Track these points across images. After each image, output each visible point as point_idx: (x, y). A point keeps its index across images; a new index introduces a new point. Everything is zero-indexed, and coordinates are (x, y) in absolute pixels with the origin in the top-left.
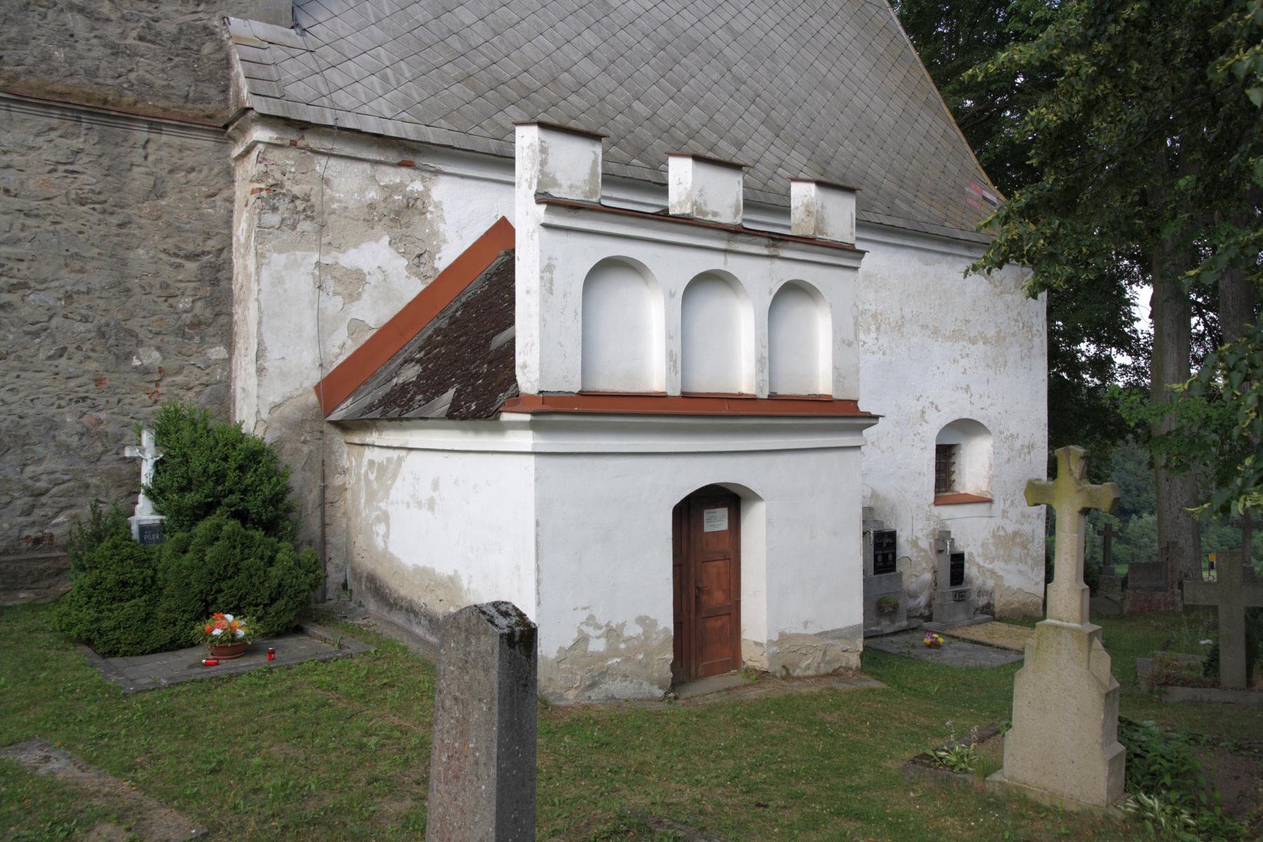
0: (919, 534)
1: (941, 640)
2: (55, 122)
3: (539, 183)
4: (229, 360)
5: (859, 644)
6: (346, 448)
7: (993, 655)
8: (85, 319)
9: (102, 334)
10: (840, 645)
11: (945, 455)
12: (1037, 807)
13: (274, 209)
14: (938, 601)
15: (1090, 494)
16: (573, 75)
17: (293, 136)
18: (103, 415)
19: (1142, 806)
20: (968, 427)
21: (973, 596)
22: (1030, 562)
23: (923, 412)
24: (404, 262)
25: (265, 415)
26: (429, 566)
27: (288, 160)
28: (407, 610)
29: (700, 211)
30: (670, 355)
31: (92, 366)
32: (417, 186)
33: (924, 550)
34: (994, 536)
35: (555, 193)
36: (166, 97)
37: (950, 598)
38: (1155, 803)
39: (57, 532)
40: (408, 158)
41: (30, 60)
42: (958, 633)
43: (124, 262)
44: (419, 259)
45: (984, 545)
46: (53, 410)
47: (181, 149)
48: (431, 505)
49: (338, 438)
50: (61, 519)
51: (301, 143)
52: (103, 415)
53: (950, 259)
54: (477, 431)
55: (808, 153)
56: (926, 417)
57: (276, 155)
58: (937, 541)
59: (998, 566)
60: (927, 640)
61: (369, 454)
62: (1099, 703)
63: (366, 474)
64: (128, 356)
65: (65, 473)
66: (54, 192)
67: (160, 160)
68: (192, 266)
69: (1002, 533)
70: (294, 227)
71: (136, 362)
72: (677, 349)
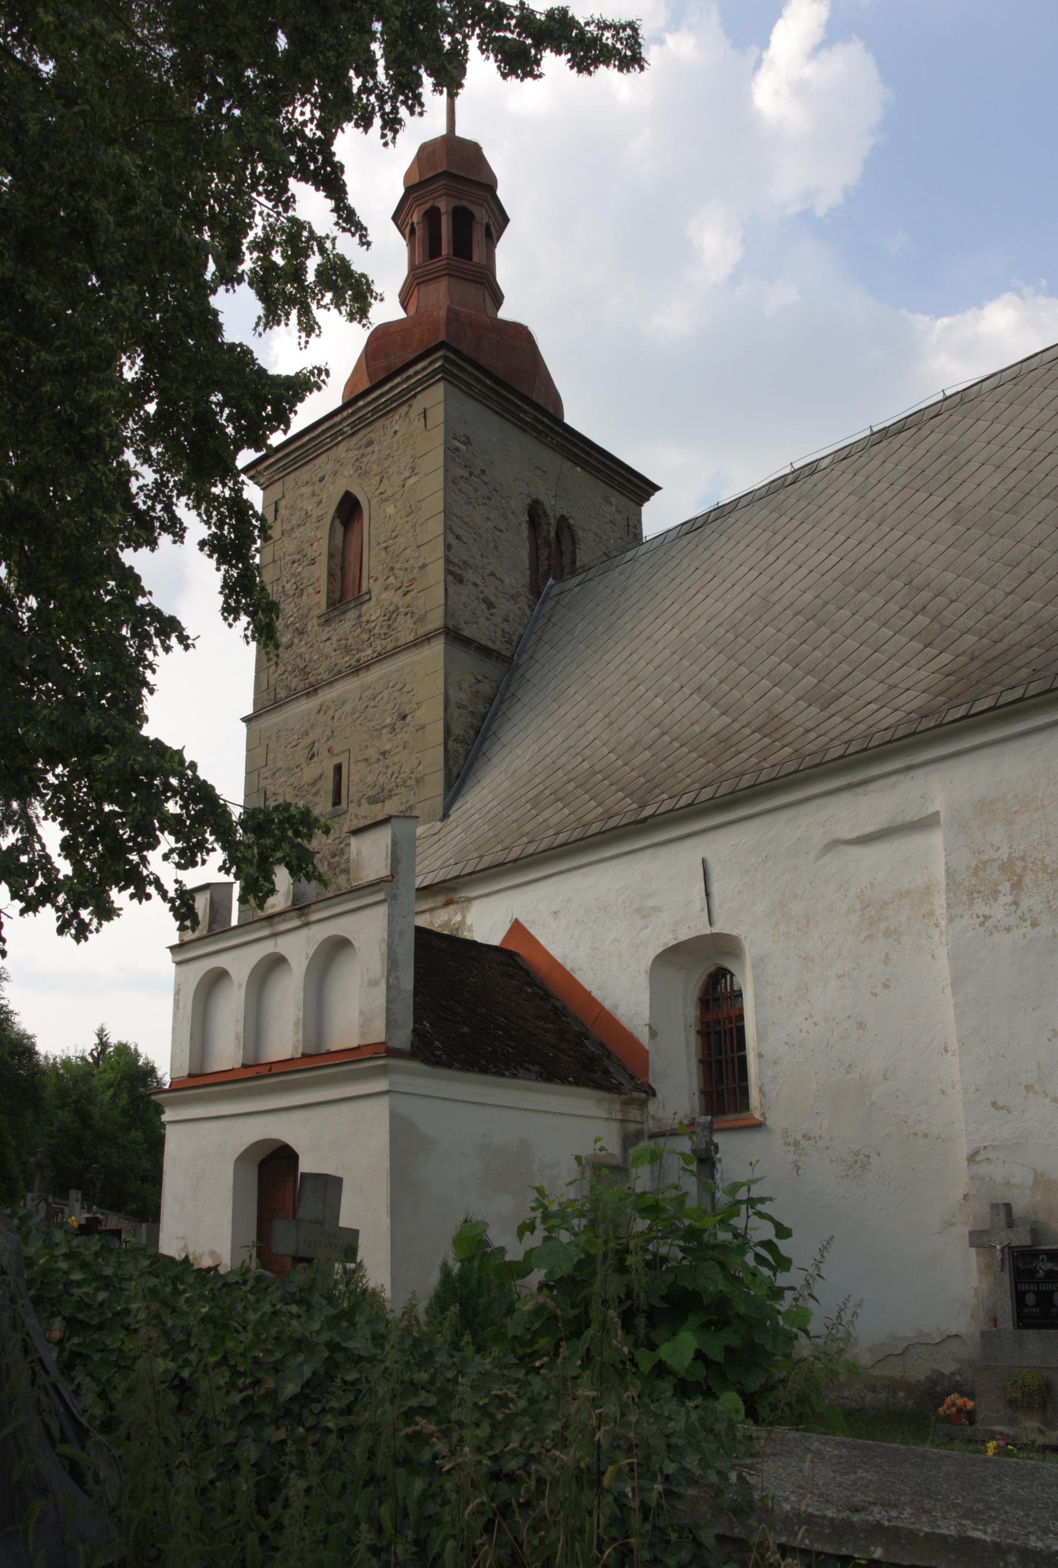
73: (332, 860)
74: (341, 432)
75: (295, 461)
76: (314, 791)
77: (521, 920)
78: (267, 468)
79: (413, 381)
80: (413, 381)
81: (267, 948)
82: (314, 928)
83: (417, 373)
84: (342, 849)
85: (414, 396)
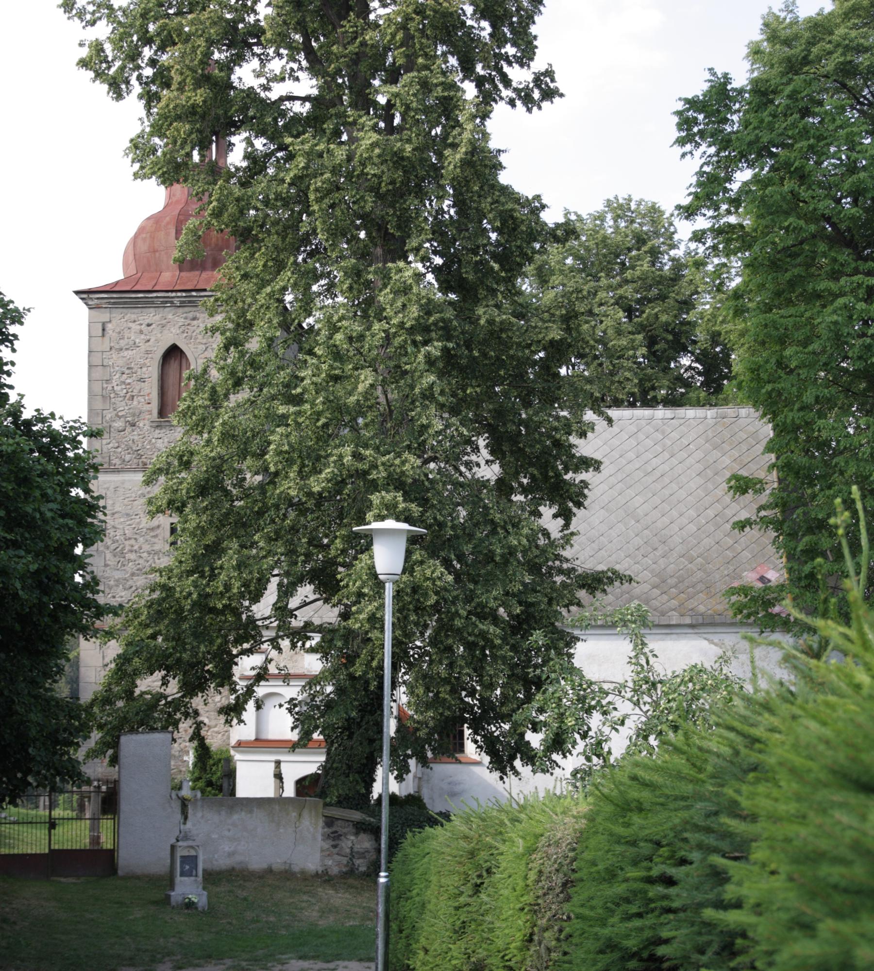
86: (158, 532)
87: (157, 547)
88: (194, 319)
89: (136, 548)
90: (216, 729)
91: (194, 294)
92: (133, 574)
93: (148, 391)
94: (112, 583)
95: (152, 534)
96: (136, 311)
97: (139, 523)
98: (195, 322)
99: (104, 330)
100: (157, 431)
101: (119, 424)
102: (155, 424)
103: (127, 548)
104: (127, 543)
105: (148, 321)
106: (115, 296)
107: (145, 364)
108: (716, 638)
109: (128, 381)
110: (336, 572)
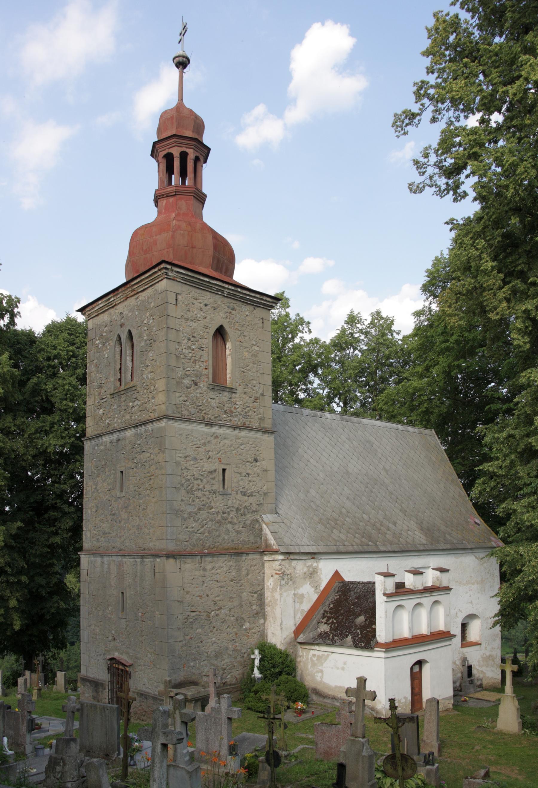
0: (456, 659)
1: (467, 699)
2: (226, 558)
3: (384, 591)
4: (264, 623)
5: (452, 701)
6: (301, 649)
7: (485, 703)
8: (233, 616)
9: (237, 620)
10: (448, 702)
11: (464, 626)
12: (505, 734)
13: (284, 579)
14: (463, 684)
15: (513, 668)
16: (345, 509)
17: (287, 556)
18: (237, 644)
19: (525, 732)
20: (472, 616)
21: (475, 681)
22: (495, 666)
23: (457, 614)
24: (313, 589)
25: (283, 642)
26: (342, 685)
27: (286, 563)
28: (332, 698)
29: (415, 588)
30: (409, 628)
31: (235, 630)
32: (315, 564)
33: (458, 665)
34: (482, 657)
35: (387, 592)
36: (249, 544)
37: (468, 683)
38: (527, 731)
39: (228, 680)
40: (313, 556)
41: (221, 541)
42: (471, 696)
43: (241, 597)
44: (316, 587)
45: (479, 661)
46: (227, 644)
47: (253, 559)
48: (343, 669)
49: (299, 646)
50: (229, 676)
51: (289, 558)
52: (237, 644)
53: (465, 554)
54: (363, 651)
55: (415, 520)
56: (458, 615)
57: (283, 563)
58: (463, 661)
59: (484, 669)
60: (463, 699)
61: (312, 652)
62: (516, 711)
63: (311, 658)
64: (242, 626)
65: (230, 662)
66: (226, 579)
67: (248, 565)
68: (256, 595)
69: (485, 656)
70: (288, 584)
71: (244, 627)
72: (411, 626)
73: (223, 515)
74: (222, 292)
75: (193, 282)
76: (211, 476)
77: (339, 571)
78: (178, 272)
79: (263, 302)
80: (263, 302)
81: (418, 601)
82: (432, 597)
83: (266, 301)
84: (228, 512)
85: (258, 307)
86: (215, 475)
87: (215, 488)
88: (233, 309)
89: (201, 487)
90: (253, 631)
91: (239, 290)
92: (200, 509)
93: (206, 359)
94: (186, 516)
95: (211, 476)
96: (198, 291)
97: (203, 467)
98: (233, 312)
99: (176, 299)
100: (212, 393)
101: (186, 382)
102: (211, 387)
103: (196, 487)
104: (195, 482)
105: (206, 302)
106: (190, 274)
107: (203, 336)
108: (477, 555)
109: (193, 347)
110: (38, 655)
